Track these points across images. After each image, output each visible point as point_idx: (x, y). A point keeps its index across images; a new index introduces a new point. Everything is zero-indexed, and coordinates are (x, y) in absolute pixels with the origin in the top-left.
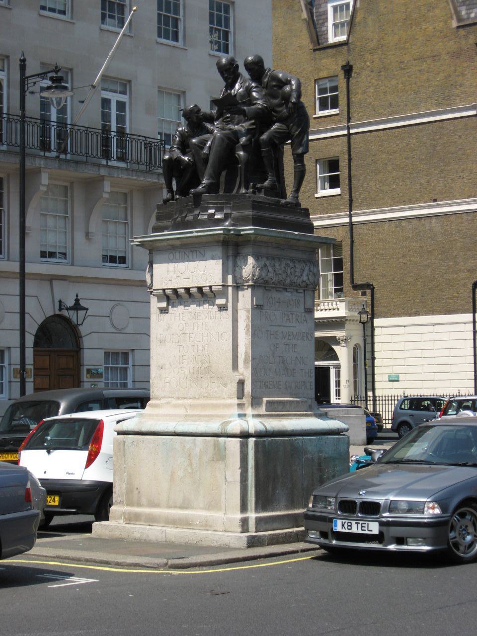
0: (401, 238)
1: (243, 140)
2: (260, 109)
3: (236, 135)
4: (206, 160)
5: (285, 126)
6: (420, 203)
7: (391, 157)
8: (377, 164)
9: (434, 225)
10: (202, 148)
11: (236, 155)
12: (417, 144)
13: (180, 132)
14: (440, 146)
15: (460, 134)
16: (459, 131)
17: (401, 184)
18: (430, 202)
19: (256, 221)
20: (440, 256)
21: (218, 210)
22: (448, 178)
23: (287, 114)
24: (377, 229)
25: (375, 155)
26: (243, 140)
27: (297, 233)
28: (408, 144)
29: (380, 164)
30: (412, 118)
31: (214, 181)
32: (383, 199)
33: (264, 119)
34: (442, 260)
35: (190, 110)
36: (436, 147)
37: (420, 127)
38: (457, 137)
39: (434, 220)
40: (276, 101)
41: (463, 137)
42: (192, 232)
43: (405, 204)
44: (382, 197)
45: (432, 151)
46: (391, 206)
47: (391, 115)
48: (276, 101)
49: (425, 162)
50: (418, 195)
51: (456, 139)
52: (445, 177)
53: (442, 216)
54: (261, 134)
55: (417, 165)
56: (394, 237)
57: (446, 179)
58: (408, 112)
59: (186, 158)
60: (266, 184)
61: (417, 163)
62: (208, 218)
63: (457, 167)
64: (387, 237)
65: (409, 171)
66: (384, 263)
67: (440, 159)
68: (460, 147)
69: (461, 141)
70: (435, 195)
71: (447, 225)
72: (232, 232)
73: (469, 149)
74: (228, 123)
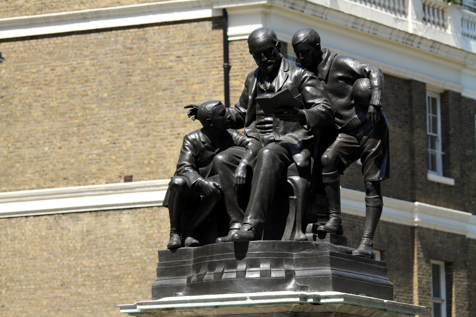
0: (59, 250)
1: (299, 158)
2: (322, 112)
3: (290, 149)
4: (244, 190)
5: (355, 139)
6: (97, 183)
7: (39, 92)
8: (11, 104)
9: (127, 226)
10: (234, 169)
11: (289, 181)
12: (93, 68)
13: (192, 141)
14: (139, 74)
15: (180, 53)
16: (177, 46)
17: (59, 145)
18: (119, 182)
19: (338, 283)
20: (137, 286)
21: (277, 263)
22: (154, 136)
23: (359, 121)
24: (10, 231)
25: (7, 87)
26: (299, 158)
27: (385, 301)
28: (76, 68)
29: (17, 106)
30: (85, 18)
31: (262, 221)
32: (23, 173)
33: (324, 130)
34: (141, 293)
35: (212, 110)
36: (131, 76)
37: (100, 36)
38: (173, 58)
39: (126, 217)
40: (343, 101)
41: (185, 59)
42: (245, 299)
43: (67, 185)
44: (21, 169)
45: (123, 84)
46: (39, 187)
47: (40, 10)
48: (343, 101)
49: (107, 104)
50: (93, 168)
51: (172, 61)
52: (148, 135)
53: (142, 210)
54: (323, 151)
55: (93, 109)
56: (44, 247)
57: (150, 138)
58: (76, 7)
59: (211, 183)
60: (329, 224)
61: (94, 106)
62: (261, 276)
63: (172, 116)
64: (30, 247)
65: (77, 121)
66: (23, 297)
67: (139, 99)
68: (179, 78)
69: (181, 66)
70: (128, 167)
71: (153, 226)
72: (310, 300)
73: (198, 83)
74: (265, 130)
